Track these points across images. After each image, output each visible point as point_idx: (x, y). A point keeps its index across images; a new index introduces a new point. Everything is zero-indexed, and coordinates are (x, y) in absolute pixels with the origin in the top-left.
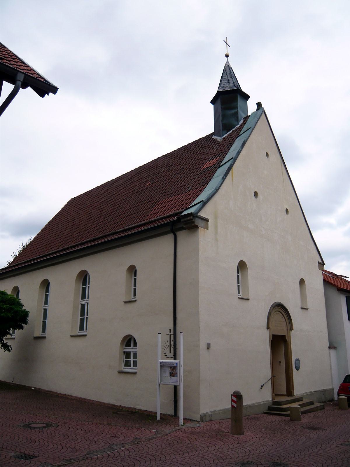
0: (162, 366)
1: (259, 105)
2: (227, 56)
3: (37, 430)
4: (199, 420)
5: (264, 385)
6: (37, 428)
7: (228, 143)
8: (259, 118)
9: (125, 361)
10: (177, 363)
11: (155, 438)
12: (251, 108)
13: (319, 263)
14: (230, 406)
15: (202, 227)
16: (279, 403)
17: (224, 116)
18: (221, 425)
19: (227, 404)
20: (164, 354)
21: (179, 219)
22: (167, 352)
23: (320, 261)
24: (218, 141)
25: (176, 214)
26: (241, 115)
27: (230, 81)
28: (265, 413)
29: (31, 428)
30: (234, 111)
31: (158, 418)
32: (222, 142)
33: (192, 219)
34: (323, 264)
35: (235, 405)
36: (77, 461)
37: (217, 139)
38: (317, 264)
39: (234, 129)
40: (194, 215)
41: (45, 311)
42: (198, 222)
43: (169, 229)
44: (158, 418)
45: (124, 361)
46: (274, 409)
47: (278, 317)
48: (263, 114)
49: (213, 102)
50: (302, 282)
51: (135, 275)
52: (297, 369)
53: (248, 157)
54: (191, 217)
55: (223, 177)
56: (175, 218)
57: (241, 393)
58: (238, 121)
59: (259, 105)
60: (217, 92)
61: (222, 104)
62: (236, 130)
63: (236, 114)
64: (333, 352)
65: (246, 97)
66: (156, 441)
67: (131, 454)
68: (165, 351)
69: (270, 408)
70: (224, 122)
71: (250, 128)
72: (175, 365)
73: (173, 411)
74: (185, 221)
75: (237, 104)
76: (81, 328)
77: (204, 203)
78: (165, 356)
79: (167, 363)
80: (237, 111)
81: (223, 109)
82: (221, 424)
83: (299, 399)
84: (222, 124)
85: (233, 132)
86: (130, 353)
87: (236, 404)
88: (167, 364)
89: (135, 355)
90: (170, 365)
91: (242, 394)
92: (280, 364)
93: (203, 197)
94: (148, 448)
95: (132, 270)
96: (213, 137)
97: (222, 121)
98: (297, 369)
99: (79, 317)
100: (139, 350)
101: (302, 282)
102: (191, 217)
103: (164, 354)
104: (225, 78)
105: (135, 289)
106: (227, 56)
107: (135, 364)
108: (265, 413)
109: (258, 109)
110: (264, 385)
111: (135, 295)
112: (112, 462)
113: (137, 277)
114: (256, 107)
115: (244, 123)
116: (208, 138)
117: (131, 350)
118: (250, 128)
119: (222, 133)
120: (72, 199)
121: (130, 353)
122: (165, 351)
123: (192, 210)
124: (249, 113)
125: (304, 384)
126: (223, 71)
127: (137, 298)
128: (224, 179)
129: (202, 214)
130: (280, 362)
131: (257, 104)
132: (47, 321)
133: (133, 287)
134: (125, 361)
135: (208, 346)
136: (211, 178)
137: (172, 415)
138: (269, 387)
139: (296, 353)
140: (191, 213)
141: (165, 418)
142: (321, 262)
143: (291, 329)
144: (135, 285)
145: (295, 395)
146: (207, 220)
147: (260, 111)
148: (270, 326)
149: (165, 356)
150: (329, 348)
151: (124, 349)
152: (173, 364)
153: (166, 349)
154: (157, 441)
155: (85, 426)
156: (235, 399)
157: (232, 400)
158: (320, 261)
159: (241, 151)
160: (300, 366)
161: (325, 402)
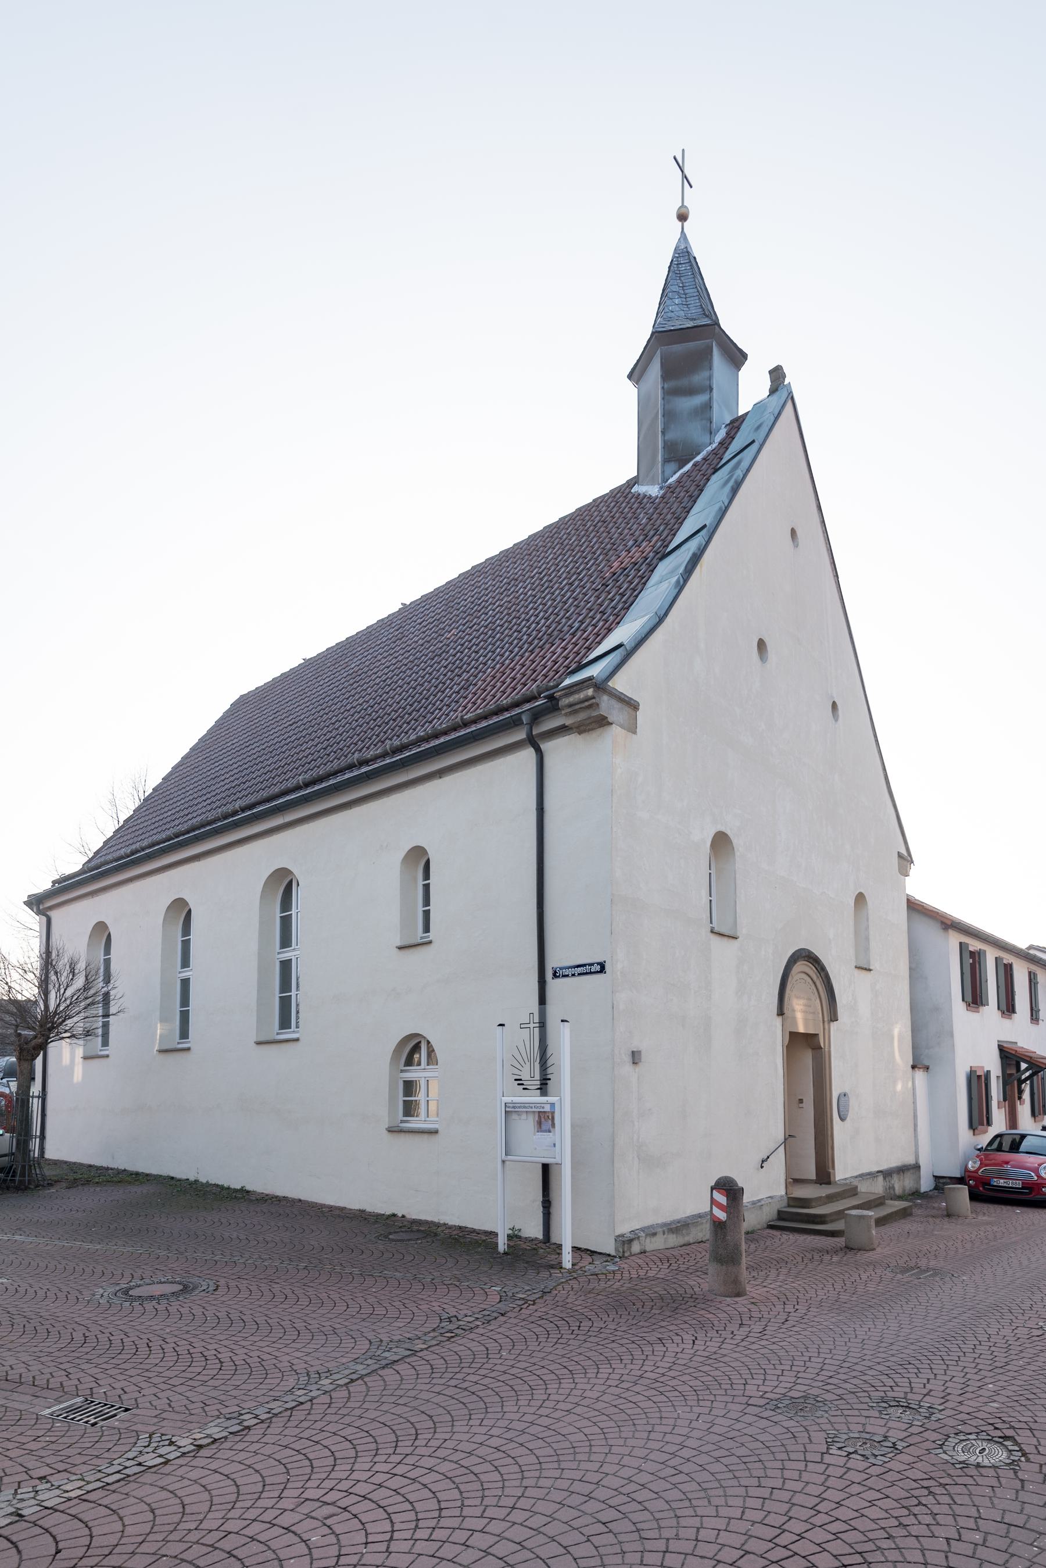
1: (777, 375)
2: (682, 217)
3: (149, 1306)
4: (613, 1253)
6: (151, 1298)
7: (686, 495)
8: (779, 414)
10: (553, 1105)
11: (502, 1315)
12: (751, 389)
13: (900, 855)
15: (622, 726)
16: (804, 1203)
17: (670, 416)
18: (674, 1266)
22: (525, 1075)
23: (904, 852)
24: (650, 497)
26: (721, 417)
27: (691, 301)
28: (771, 1227)
29: (133, 1299)
30: (699, 400)
31: (502, 1245)
32: (663, 497)
35: (722, 1215)
36: (262, 1422)
38: (895, 859)
39: (699, 458)
40: (600, 686)
41: (185, 983)
42: (607, 706)
43: (521, 735)
44: (502, 1245)
46: (793, 1218)
48: (789, 404)
49: (636, 375)
50: (860, 899)
51: (427, 875)
52: (842, 1119)
53: (747, 523)
54: (590, 692)
55: (678, 581)
57: (736, 1184)
58: (711, 433)
59: (777, 375)
60: (653, 334)
61: (667, 374)
62: (705, 459)
63: (708, 406)
64: (920, 1075)
65: (737, 357)
66: (505, 1322)
67: (439, 1375)
68: (517, 1072)
69: (781, 1215)
70: (669, 436)
71: (753, 442)
72: (547, 1108)
73: (541, 1228)
74: (570, 705)
75: (710, 378)
76: (285, 1023)
77: (627, 653)
79: (524, 1105)
80: (710, 399)
81: (669, 393)
82: (672, 1261)
83: (851, 1191)
84: (665, 442)
85: (695, 465)
91: (740, 1185)
93: (623, 633)
94: (487, 1349)
95: (419, 861)
96: (636, 489)
97: (663, 433)
99: (277, 995)
101: (860, 899)
102: (590, 692)
104: (675, 288)
105: (427, 914)
106: (682, 217)
108: (771, 1227)
109: (773, 391)
111: (427, 929)
112: (379, 1413)
113: (433, 881)
114: (767, 384)
115: (730, 437)
116: (622, 495)
118: (753, 442)
119: (663, 472)
120: (242, 696)
122: (517, 1072)
123: (594, 671)
124: (744, 407)
125: (860, 1152)
126: (670, 267)
127: (432, 935)
128: (680, 587)
129: (620, 683)
130: (801, 1101)
131: (770, 372)
132: (192, 1007)
133: (421, 909)
136: (635, 592)
138: (779, 1161)
139: (841, 1079)
140: (590, 678)
143: (834, 1017)
144: (427, 901)
146: (632, 705)
147: (782, 394)
150: (913, 1067)
151: (402, 1071)
154: (508, 1325)
155: (298, 1285)
156: (722, 1199)
157: (713, 1201)
158: (904, 852)
159: (727, 508)
161: (914, 1198)
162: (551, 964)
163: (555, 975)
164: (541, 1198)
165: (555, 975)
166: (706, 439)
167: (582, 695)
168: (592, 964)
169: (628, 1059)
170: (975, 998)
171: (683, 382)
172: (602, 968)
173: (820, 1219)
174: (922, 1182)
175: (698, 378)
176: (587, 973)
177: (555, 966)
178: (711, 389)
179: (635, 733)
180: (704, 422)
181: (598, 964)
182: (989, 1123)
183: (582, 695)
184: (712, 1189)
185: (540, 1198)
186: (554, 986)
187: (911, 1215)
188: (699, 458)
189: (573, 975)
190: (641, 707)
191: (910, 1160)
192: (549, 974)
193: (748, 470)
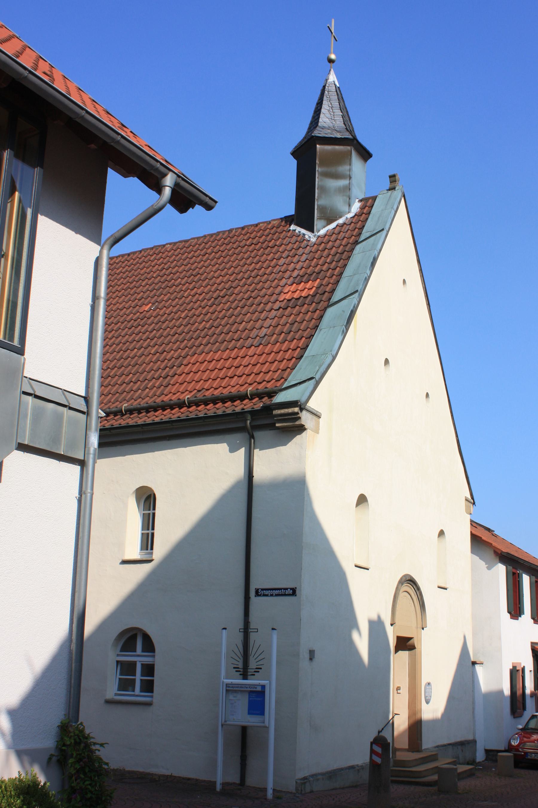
0: (230, 689)
5: (383, 729)
9: (120, 679)
10: (263, 687)
14: (367, 760)
19: (361, 756)
20: (234, 668)
21: (268, 410)
25: (260, 395)
31: (218, 788)
33: (298, 413)
34: (472, 501)
35: (378, 760)
37: (304, 234)
38: (464, 502)
39: (341, 221)
42: (305, 418)
44: (218, 788)
45: (118, 680)
47: (406, 602)
52: (427, 702)
54: (296, 410)
56: (258, 404)
63: (348, 188)
72: (259, 689)
75: (350, 170)
78: (236, 671)
83: (433, 758)
86: (134, 664)
87: (380, 760)
88: (241, 687)
89: (149, 670)
90: (250, 689)
92: (399, 691)
98: (427, 702)
100: (160, 661)
102: (296, 410)
103: (234, 668)
107: (148, 687)
110: (383, 729)
117: (139, 658)
118: (383, 230)
121: (134, 664)
134: (120, 679)
135: (312, 654)
137: (234, 783)
141: (228, 790)
142: (470, 498)
145: (423, 748)
146: (317, 415)
148: (397, 621)
149: (236, 671)
152: (256, 688)
153: (255, 657)
156: (379, 750)
157: (372, 752)
160: (431, 697)
162: (255, 585)
163: (257, 593)
164: (240, 754)
165: (257, 593)
166: (346, 208)
167: (290, 410)
168: (286, 589)
169: (307, 656)
170: (515, 611)
171: (332, 170)
172: (294, 592)
173: (419, 774)
174: (477, 754)
175: (343, 169)
176: (282, 595)
177: (258, 587)
178: (350, 178)
179: (318, 433)
180: (345, 197)
181: (291, 589)
182: (524, 708)
183: (290, 410)
184: (372, 743)
185: (239, 753)
186: (255, 601)
187: (474, 774)
188: (341, 221)
189: (272, 595)
190: (322, 417)
191: (471, 738)
192: (252, 593)
193: (380, 250)
